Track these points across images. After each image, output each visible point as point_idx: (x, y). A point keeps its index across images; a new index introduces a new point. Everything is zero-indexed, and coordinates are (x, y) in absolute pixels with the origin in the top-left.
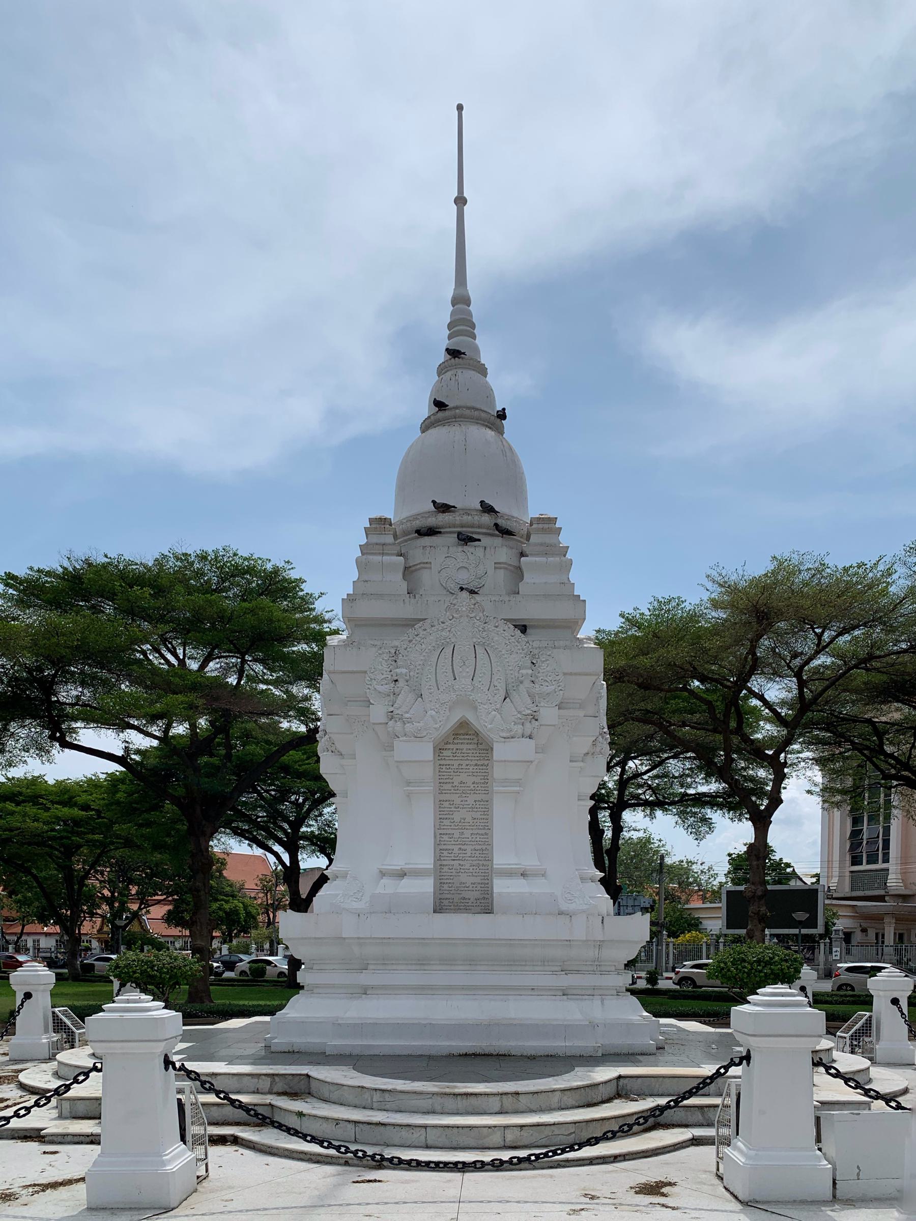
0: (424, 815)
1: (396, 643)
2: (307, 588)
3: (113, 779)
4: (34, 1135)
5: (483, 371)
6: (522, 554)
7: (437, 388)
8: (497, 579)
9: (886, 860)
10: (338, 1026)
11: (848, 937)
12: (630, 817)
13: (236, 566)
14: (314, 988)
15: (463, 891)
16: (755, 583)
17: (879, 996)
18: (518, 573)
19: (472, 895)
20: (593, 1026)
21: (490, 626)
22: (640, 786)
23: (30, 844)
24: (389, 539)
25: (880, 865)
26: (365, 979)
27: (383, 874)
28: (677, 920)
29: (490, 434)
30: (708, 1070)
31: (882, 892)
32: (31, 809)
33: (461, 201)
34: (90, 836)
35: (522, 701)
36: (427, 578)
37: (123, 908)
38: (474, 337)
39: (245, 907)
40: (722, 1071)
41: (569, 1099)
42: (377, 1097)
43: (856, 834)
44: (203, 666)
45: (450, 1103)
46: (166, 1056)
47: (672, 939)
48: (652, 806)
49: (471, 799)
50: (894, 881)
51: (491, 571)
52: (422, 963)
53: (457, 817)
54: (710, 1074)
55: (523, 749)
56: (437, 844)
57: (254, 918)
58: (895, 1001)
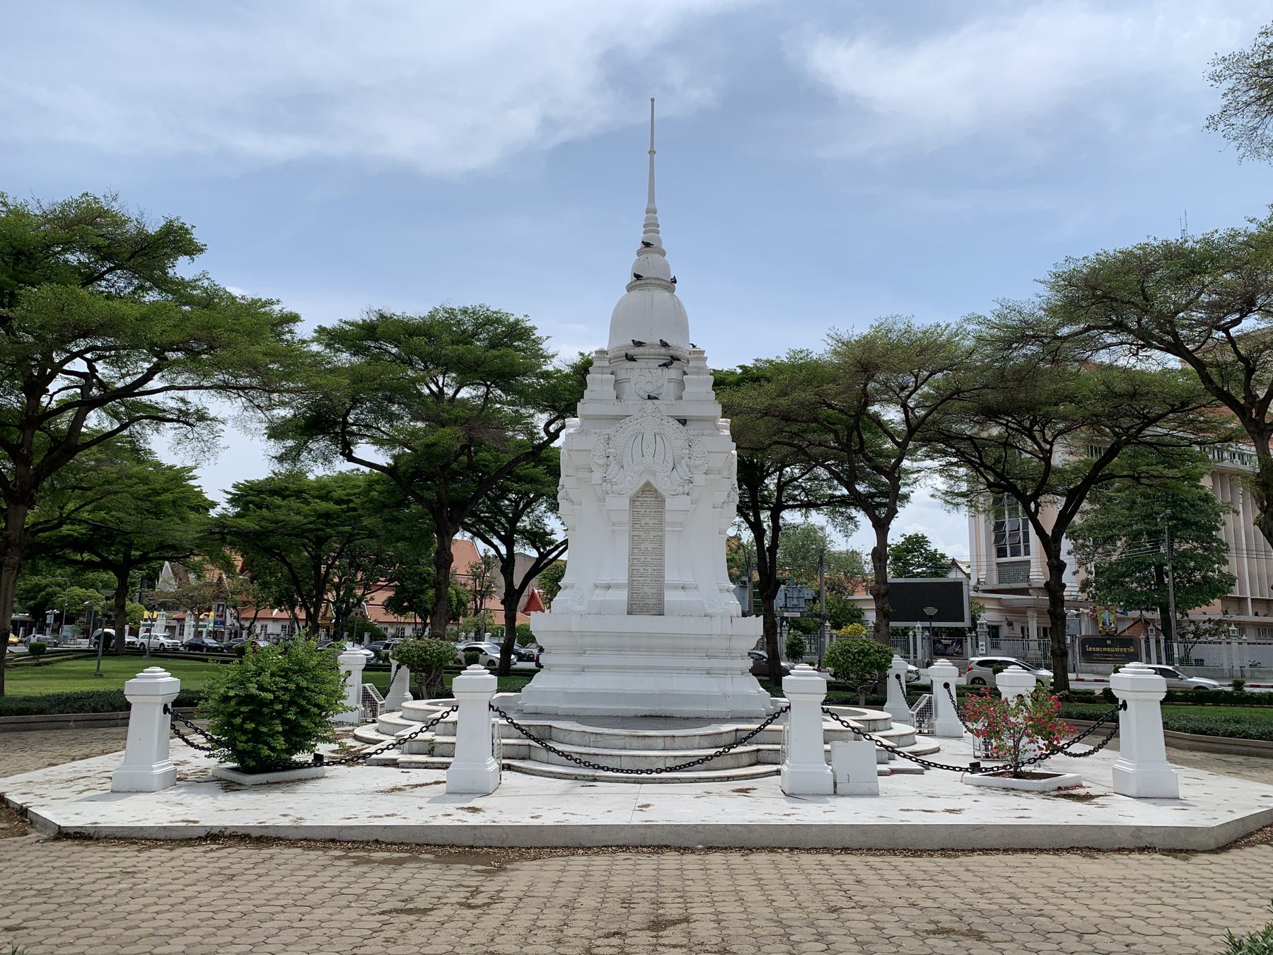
0: (623, 545)
1: (608, 431)
2: (537, 334)
3: (371, 483)
4: (393, 763)
5: (663, 253)
6: (685, 373)
7: (635, 266)
8: (671, 389)
9: (1027, 553)
10: (568, 695)
11: (994, 631)
12: (791, 517)
13: (487, 318)
14: (551, 667)
15: (646, 603)
18: (682, 385)
19: (651, 602)
20: (725, 696)
21: (664, 422)
22: (796, 488)
23: (290, 535)
24: (607, 364)
25: (1022, 558)
26: (583, 660)
27: (596, 586)
28: (842, 610)
29: (667, 294)
31: (1025, 585)
32: (294, 503)
34: (341, 528)
35: (683, 471)
36: (628, 388)
37: (350, 592)
38: (658, 232)
39: (458, 594)
41: (705, 742)
42: (668, 741)
43: (999, 527)
44: (457, 392)
45: (635, 742)
47: (834, 631)
48: (808, 506)
49: (652, 534)
51: (666, 384)
52: (620, 649)
53: (643, 547)
56: (630, 566)
57: (465, 605)
58: (946, 685)
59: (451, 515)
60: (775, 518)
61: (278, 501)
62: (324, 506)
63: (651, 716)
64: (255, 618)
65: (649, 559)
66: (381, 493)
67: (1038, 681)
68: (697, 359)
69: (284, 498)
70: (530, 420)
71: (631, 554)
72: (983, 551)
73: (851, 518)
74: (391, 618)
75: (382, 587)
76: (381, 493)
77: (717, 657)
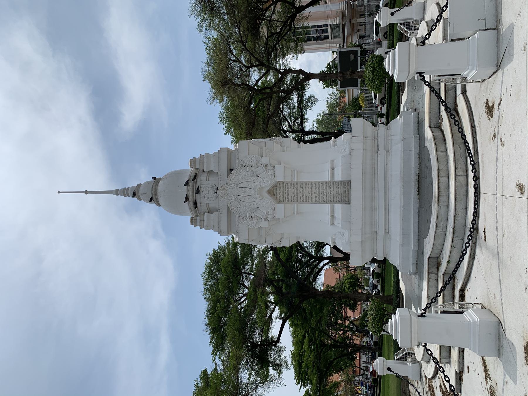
0: (306, 207)
1: (237, 216)
2: (216, 248)
3: (292, 325)
5: (140, 185)
6: (203, 171)
7: (146, 201)
8: (213, 180)
9: (326, 25)
11: (361, 37)
12: (307, 128)
13: (209, 273)
15: (342, 193)
16: (213, 87)
17: (390, 21)
18: (210, 172)
19: (342, 189)
20: (404, 139)
21: (230, 182)
22: (294, 125)
23: (320, 360)
24: (198, 218)
25: (329, 28)
26: (381, 232)
27: (333, 224)
30: (426, 89)
31: (341, 26)
32: (305, 357)
33: (86, 192)
34: (316, 336)
35: (260, 170)
36: (212, 205)
37: (348, 327)
40: (427, 83)
41: (442, 148)
42: (442, 174)
43: (315, 39)
45: (443, 198)
46: (418, 316)
47: (363, 109)
49: (300, 189)
50: (335, 22)
51: (209, 182)
52: (373, 209)
53: (308, 195)
54: (429, 89)
55: (279, 170)
56: (320, 203)
57: (353, 275)
58: (392, 14)
59: (306, 288)
60: (308, 133)
61: (304, 365)
62: (306, 344)
63: (418, 188)
64: (360, 368)
65: (315, 191)
66: (298, 319)
67: (385, 6)
68: (195, 163)
69: (303, 362)
70: (261, 251)
71: (312, 202)
72: (325, 45)
73: (309, 99)
74: (359, 307)
75: (345, 312)
76: (298, 319)
77: (378, 146)
